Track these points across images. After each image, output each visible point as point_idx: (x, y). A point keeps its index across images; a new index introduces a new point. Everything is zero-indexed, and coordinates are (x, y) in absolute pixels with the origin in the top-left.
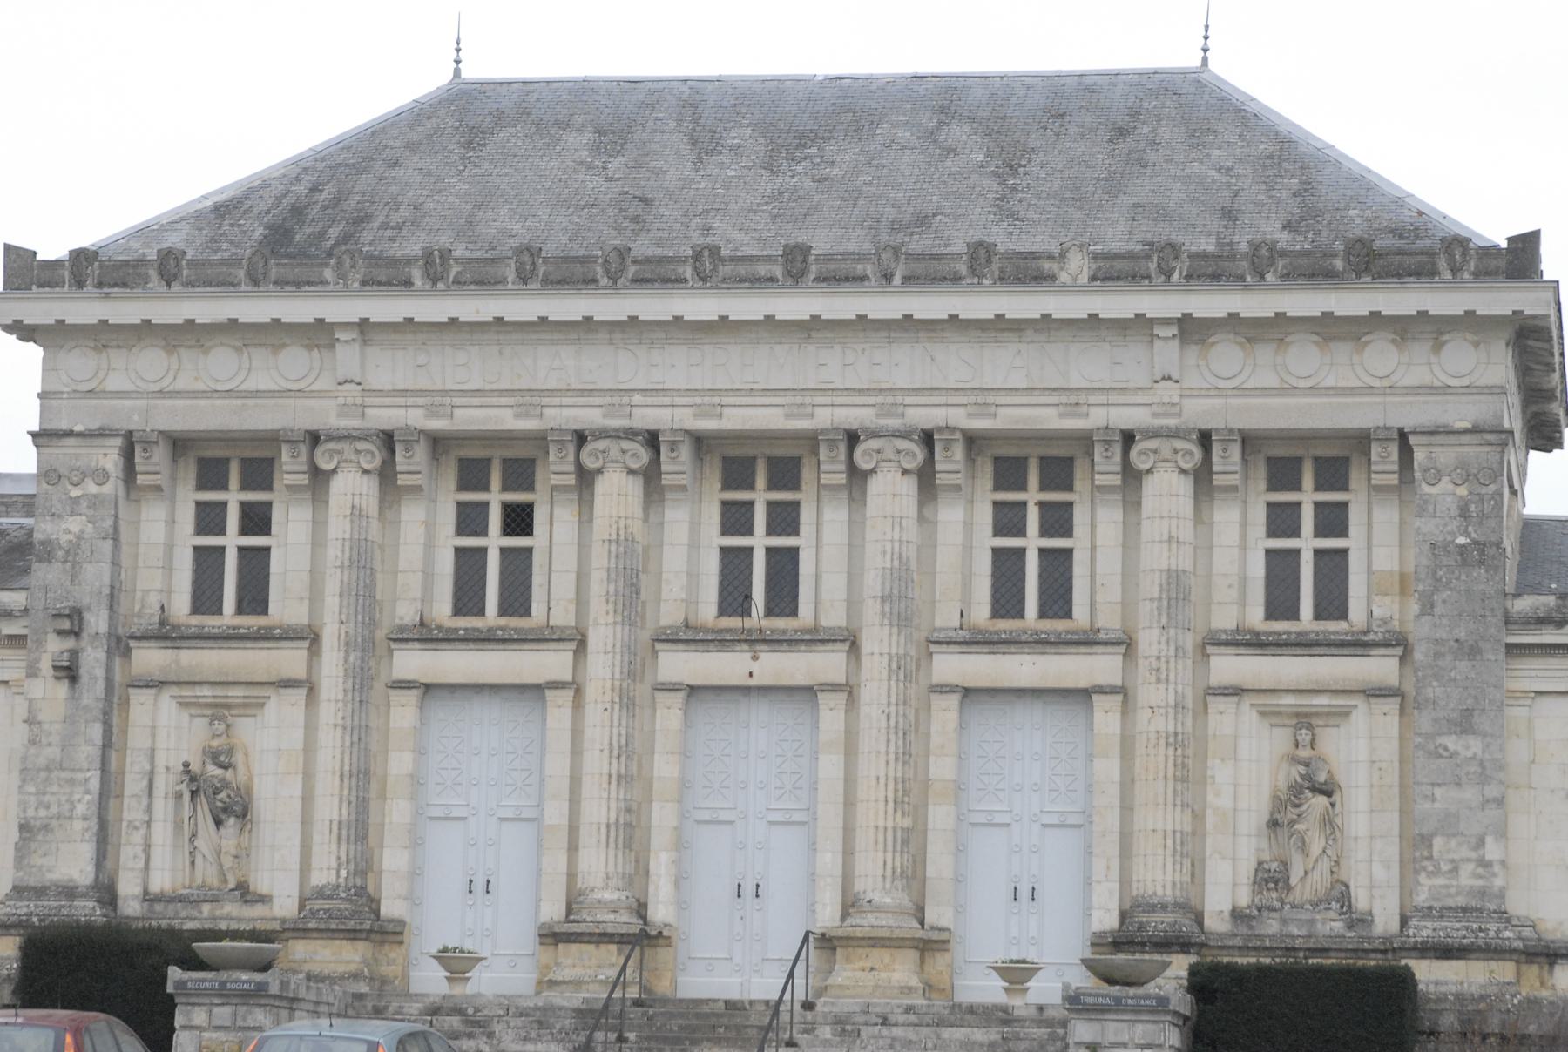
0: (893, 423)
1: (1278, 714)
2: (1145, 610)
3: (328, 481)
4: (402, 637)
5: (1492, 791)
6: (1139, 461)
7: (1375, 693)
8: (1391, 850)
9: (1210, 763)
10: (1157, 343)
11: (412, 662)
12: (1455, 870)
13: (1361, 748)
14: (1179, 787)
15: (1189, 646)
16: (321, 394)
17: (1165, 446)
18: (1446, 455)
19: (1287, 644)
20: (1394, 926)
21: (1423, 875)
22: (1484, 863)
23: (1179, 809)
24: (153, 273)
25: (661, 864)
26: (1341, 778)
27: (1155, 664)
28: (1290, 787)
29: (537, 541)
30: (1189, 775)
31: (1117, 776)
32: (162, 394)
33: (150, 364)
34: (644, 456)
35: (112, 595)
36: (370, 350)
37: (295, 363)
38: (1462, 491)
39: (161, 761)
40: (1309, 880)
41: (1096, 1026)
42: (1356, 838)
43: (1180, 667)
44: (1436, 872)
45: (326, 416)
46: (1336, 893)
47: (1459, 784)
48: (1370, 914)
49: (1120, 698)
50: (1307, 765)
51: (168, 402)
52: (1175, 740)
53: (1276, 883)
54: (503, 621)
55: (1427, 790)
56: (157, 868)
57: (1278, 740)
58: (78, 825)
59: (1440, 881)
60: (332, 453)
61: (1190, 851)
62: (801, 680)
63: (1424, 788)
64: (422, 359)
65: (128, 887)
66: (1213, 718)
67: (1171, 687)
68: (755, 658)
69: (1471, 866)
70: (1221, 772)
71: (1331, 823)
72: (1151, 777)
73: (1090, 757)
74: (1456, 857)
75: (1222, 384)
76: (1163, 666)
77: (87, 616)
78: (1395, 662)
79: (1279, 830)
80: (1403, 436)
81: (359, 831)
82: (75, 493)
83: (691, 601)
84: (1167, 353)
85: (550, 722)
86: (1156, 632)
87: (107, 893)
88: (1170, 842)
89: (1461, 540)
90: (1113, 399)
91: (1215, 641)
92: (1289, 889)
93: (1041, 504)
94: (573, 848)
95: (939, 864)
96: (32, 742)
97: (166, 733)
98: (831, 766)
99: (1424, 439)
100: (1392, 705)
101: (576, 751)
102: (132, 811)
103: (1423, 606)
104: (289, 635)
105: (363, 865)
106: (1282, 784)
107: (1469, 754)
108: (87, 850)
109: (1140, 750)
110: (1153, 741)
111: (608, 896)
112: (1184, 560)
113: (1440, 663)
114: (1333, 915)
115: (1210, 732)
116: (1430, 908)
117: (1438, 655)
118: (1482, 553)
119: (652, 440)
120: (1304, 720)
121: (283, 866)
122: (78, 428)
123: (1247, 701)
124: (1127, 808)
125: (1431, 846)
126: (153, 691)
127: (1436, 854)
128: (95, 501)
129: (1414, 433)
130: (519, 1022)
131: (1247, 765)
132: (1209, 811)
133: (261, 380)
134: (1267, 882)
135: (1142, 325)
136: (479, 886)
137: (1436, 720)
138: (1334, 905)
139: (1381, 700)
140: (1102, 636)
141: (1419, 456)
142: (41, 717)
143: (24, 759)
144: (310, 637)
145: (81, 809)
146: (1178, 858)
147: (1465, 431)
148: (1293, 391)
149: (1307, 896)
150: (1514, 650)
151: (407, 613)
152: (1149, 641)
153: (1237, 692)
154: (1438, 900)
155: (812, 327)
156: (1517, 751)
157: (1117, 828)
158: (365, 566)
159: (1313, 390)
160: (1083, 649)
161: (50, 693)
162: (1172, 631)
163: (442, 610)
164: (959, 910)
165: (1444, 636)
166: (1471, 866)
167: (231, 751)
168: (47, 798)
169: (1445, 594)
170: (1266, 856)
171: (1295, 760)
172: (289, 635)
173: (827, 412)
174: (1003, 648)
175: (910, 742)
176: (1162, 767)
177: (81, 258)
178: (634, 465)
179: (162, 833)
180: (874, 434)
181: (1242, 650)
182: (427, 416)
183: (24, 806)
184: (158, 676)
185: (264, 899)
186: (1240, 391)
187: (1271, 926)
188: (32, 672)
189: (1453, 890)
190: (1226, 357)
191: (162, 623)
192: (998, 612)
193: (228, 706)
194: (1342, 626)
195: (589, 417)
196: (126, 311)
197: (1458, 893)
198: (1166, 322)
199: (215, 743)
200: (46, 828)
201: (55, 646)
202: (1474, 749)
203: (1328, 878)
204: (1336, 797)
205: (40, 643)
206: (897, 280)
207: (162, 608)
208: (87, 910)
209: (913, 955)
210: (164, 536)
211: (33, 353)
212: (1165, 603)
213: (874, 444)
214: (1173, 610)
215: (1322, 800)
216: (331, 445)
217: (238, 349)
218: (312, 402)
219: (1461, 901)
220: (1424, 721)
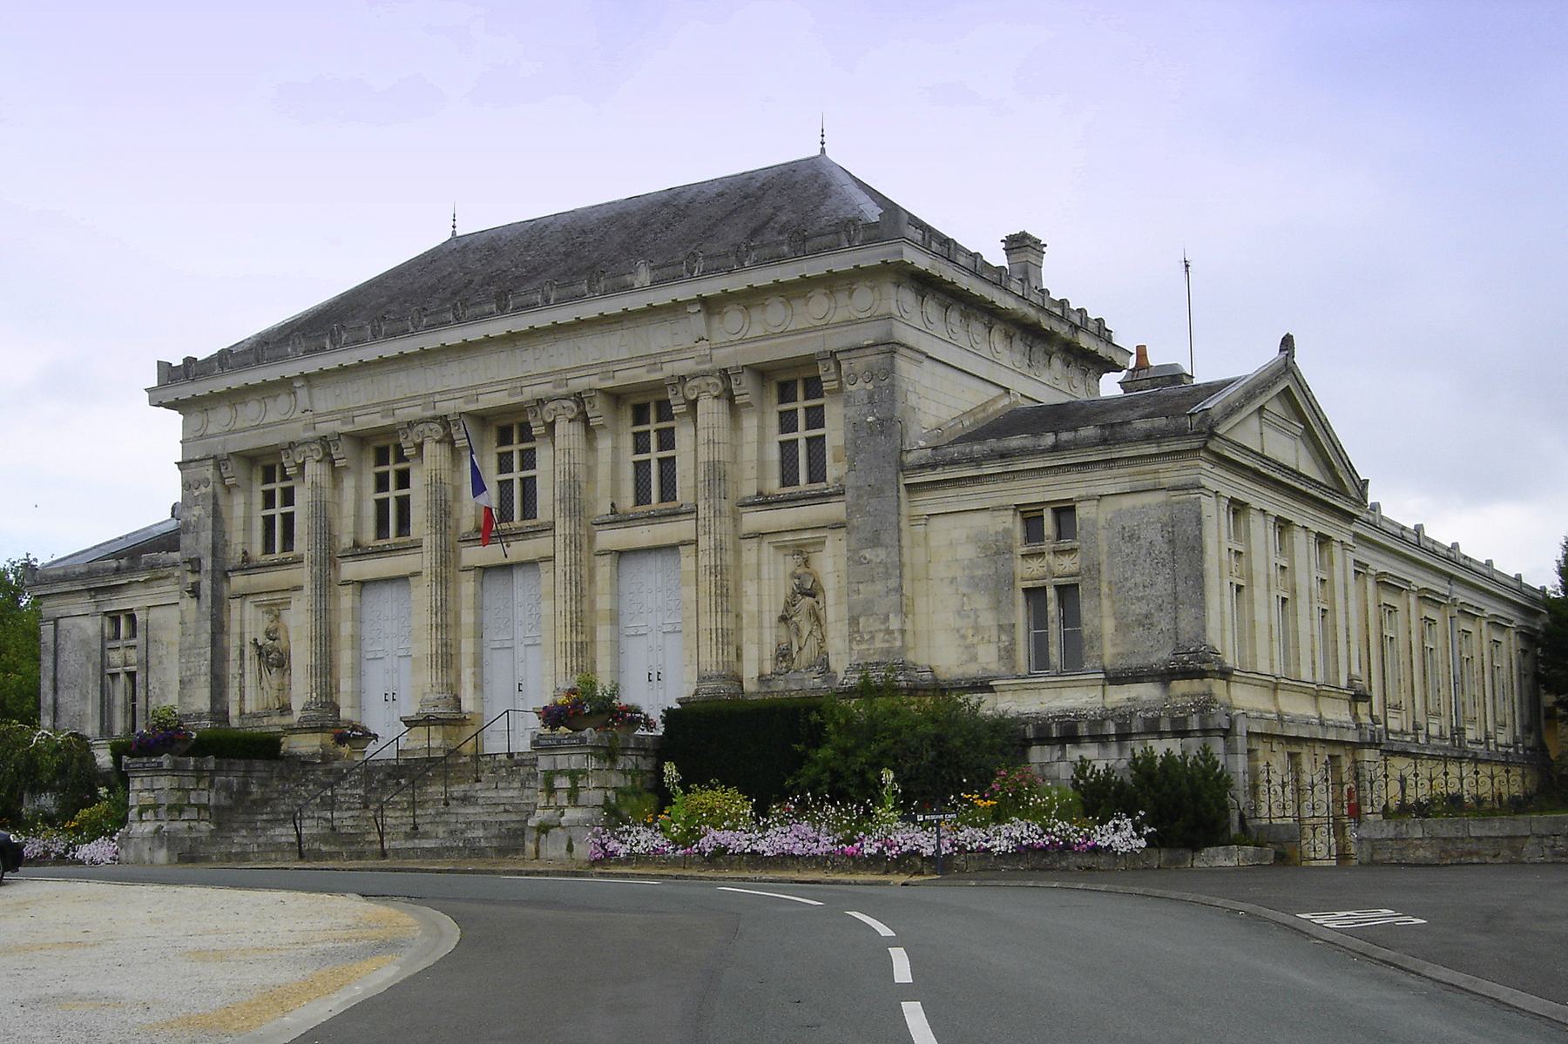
0: (562, 391)
7: (837, 526)
11: (351, 569)
12: (873, 638)
13: (830, 564)
16: (295, 421)
18: (859, 365)
22: (889, 632)
25: (345, 685)
30: (726, 592)
32: (230, 432)
36: (315, 391)
38: (870, 386)
57: (789, 564)
58: (203, 678)
59: (864, 646)
61: (729, 639)
80: (833, 354)
81: (583, 650)
84: (697, 322)
87: (219, 713)
89: (870, 419)
90: (675, 357)
93: (657, 431)
99: (845, 355)
100: (842, 533)
102: (233, 669)
112: (723, 454)
117: (859, 496)
118: (882, 425)
123: (767, 539)
131: (766, 582)
135: (676, 307)
147: (868, 346)
151: (749, 490)
153: (759, 535)
155: (511, 338)
156: (914, 556)
161: (189, 604)
163: (773, 485)
175: (580, 589)
179: (250, 680)
186: (743, 341)
187: (780, 685)
190: (733, 319)
194: (824, 485)
196: (254, 377)
204: (820, 598)
207: (245, 553)
211: (175, 419)
215: (808, 600)
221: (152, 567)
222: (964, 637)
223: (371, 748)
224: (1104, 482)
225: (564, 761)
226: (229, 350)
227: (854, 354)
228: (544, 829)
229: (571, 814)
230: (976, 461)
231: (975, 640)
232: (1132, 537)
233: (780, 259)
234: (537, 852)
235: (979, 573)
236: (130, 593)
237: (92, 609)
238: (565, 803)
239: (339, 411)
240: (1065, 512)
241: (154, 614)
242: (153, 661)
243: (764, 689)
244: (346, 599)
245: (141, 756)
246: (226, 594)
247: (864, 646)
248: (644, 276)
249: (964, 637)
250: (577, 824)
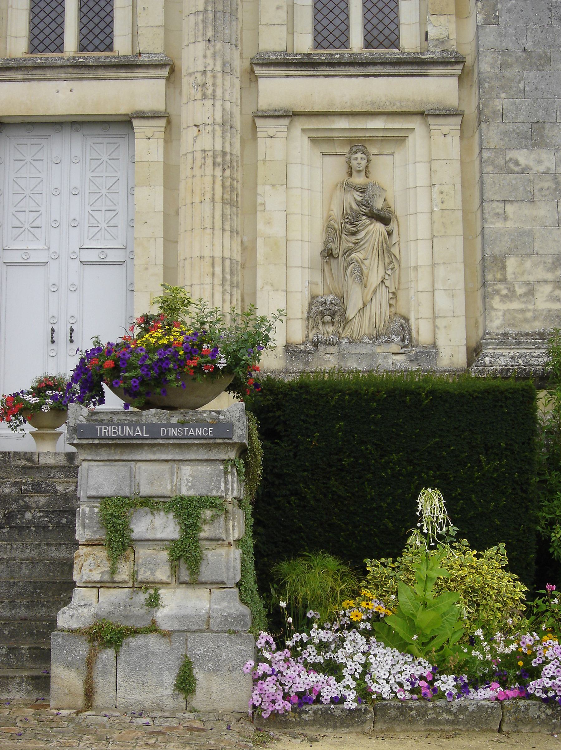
1: (330, 140)
2: (189, 26)
8: (454, 277)
9: (260, 189)
12: (531, 293)
13: (420, 176)
14: (228, 211)
15: (237, 64)
20: (461, 359)
21: (497, 298)
23: (228, 234)
26: (398, 210)
27: (200, 79)
28: (345, 215)
30: (238, 201)
31: (160, 205)
40: (366, 311)
41: (121, 470)
42: (416, 268)
43: (228, 84)
44: (511, 296)
46: (396, 326)
47: (532, 201)
48: (434, 346)
49: (162, 123)
50: (363, 191)
52: (223, 161)
53: (333, 315)
55: (498, 207)
59: (515, 305)
61: (240, 271)
63: (495, 205)
66: (262, 143)
67: (218, 103)
69: (548, 289)
70: (271, 199)
71: (389, 251)
72: (197, 200)
74: (531, 278)
76: (210, 81)
79: (333, 262)
86: (201, 46)
88: (218, 270)
92: (346, 322)
100: (451, 126)
103: (487, 16)
106: (336, 212)
107: (542, 169)
109: (185, 172)
110: (199, 162)
113: (507, 74)
114: (394, 348)
115: (260, 157)
116: (505, 335)
117: (504, 66)
123: (300, 124)
124: (170, 241)
125: (504, 268)
126: (286, 122)
127: (510, 277)
131: (300, 191)
132: (260, 241)
134: (322, 314)
137: (505, 133)
138: (396, 339)
139: (441, 120)
140: (144, 59)
146: (228, 288)
149: (366, 329)
152: (194, 57)
153: (291, 115)
154: (514, 325)
157: (160, 260)
160: (123, 73)
162: (219, 45)
165: (511, 46)
166: (548, 289)
170: (320, 290)
171: (349, 187)
174: (38, 74)
176: (209, 189)
181: (292, 71)
187: (327, 363)
189: (529, 315)
197: (535, 318)
202: (546, 164)
203: (386, 311)
204: (393, 226)
212: (210, 15)
214: (219, 22)
215: (378, 227)
219: (538, 326)
220: (493, 134)
225: (153, 476)
228: (108, 636)
229: (177, 603)
234: (89, 693)
238: (162, 574)
243: (298, 366)
245: (256, 568)
250: (206, 626)
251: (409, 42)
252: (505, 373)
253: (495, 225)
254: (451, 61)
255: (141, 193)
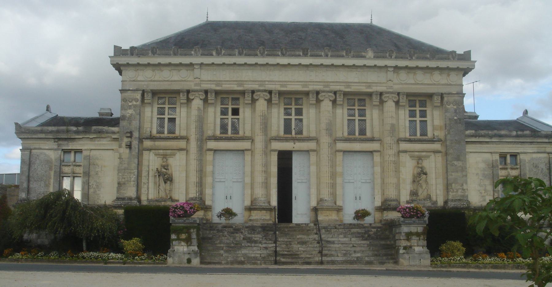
0: (327, 89)
3: (384, 104)
4: (210, 138)
5: (464, 173)
6: (255, 97)
7: (435, 152)
10: (388, 72)
11: (212, 144)
12: (457, 191)
17: (391, 96)
18: (451, 99)
19: (417, 141)
22: (463, 189)
24: (150, 52)
26: (428, 172)
29: (241, 116)
32: (151, 81)
33: (148, 74)
34: (268, 96)
35: (139, 129)
36: (202, 71)
37: (184, 74)
38: (455, 107)
39: (151, 168)
40: (422, 194)
44: (453, 192)
45: (192, 86)
47: (457, 172)
51: (153, 83)
54: (232, 135)
56: (151, 193)
59: (454, 194)
60: (193, 95)
62: (306, 149)
64: (215, 73)
65: (144, 198)
68: (295, 144)
70: (402, 169)
73: (373, 167)
75: (403, 82)
77: (133, 133)
78: (250, 143)
81: (201, 184)
82: (130, 104)
83: (278, 131)
85: (311, 159)
87: (138, 199)
89: (455, 118)
91: (399, 140)
92: (418, 196)
94: (252, 188)
95: (339, 192)
96: (121, 163)
97: (152, 161)
98: (313, 169)
100: (440, 155)
101: (252, 166)
102: (144, 180)
104: (182, 138)
105: (201, 192)
106: (415, 172)
108: (134, 189)
111: (262, 199)
112: (394, 121)
119: (270, 92)
120: (420, 158)
121: (181, 193)
122: (131, 89)
123: (408, 153)
128: (135, 106)
129: (445, 94)
130: (248, 229)
133: (176, 78)
136: (229, 197)
141: (445, 99)
142: (123, 157)
143: (118, 167)
144: (186, 138)
145: (133, 179)
148: (418, 84)
150: (468, 142)
153: (405, 152)
158: (201, 121)
159: (422, 84)
161: (125, 151)
164: (343, 201)
167: (168, 166)
168: (124, 177)
169: (453, 130)
171: (419, 167)
172: (182, 138)
173: (375, 87)
177: (133, 49)
178: (267, 98)
179: (151, 185)
180: (324, 92)
182: (345, 88)
183: (119, 178)
184: (150, 148)
185: (177, 201)
188: (120, 147)
191: (151, 135)
192: (286, 132)
193: (166, 155)
194: (427, 137)
195: (255, 87)
196: (144, 60)
198: (391, 67)
199: (164, 164)
200: (124, 184)
201: (126, 140)
205: (122, 140)
206: (329, 56)
208: (135, 202)
209: (336, 212)
210: (150, 114)
213: (323, 94)
215: (425, 176)
216: (193, 93)
217: (170, 71)
218: (188, 83)
219: (459, 198)
221: (99, 132)
222: (481, 193)
223: (236, 218)
224: (529, 148)
226: (136, 48)
227: (450, 95)
230: (491, 137)
231: (485, 194)
232: (536, 167)
233: (426, 59)
235: (486, 173)
236: (81, 142)
237: (56, 147)
239: (214, 81)
240: (514, 156)
241: (93, 153)
242: (92, 173)
244: (209, 156)
246: (205, 148)
247: (454, 194)
248: (370, 54)
249: (481, 193)
251: (430, 135)
252: (453, 208)
253: (450, 177)
254: (439, 140)
255: (376, 168)
